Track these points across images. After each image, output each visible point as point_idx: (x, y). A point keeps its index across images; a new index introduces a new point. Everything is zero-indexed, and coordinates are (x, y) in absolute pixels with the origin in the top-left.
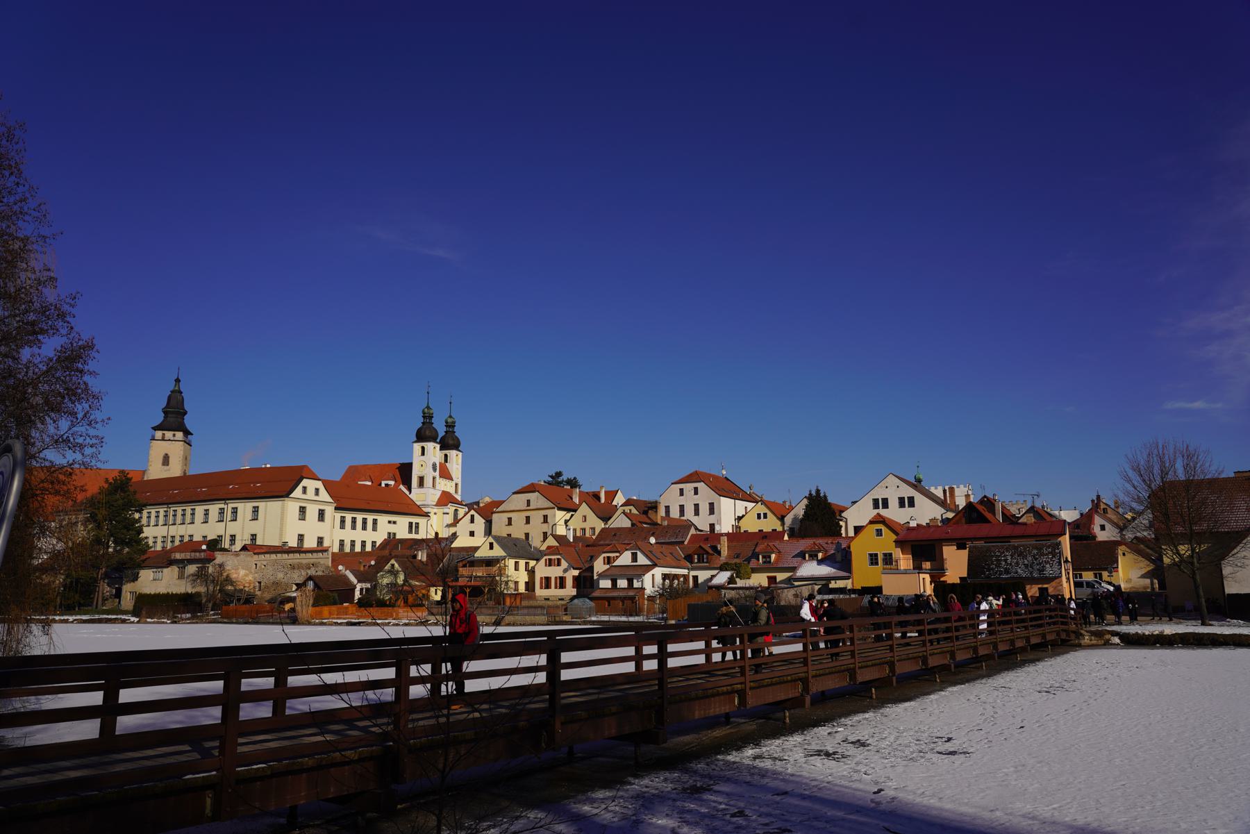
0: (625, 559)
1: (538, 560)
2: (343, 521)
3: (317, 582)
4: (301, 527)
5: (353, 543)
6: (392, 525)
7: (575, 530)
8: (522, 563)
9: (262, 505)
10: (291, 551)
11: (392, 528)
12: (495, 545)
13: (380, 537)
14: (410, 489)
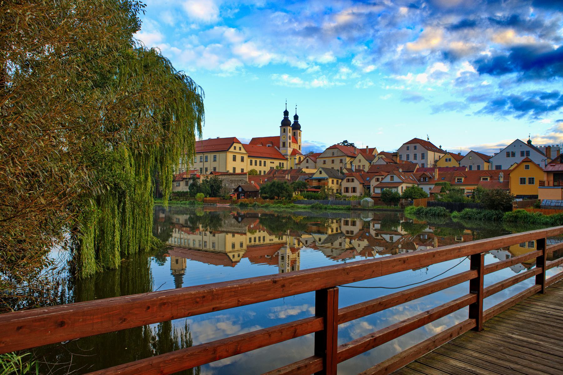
0: (388, 179)
1: (342, 179)
2: (251, 161)
3: (243, 188)
4: (234, 164)
5: (260, 172)
6: (272, 164)
7: (355, 166)
8: (335, 181)
9: (217, 155)
10: (231, 174)
11: (272, 165)
12: (323, 172)
13: (267, 169)
14: (279, 148)
